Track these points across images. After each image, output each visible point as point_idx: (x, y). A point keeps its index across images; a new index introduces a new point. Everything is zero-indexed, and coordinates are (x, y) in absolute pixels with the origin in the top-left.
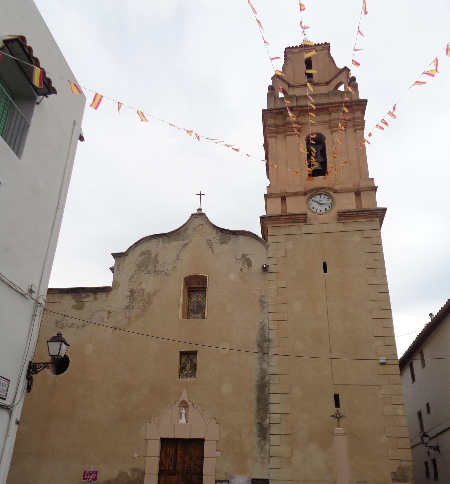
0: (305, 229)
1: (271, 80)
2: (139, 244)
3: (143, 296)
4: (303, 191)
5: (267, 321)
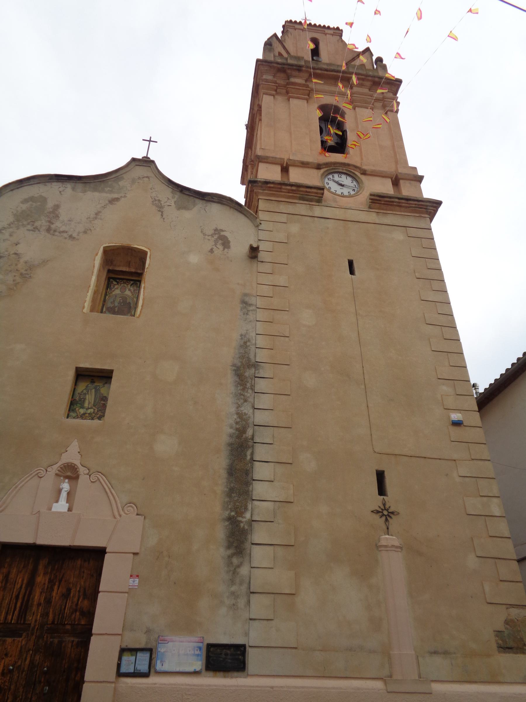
0: (318, 211)
3: (16, 265)
4: (316, 163)
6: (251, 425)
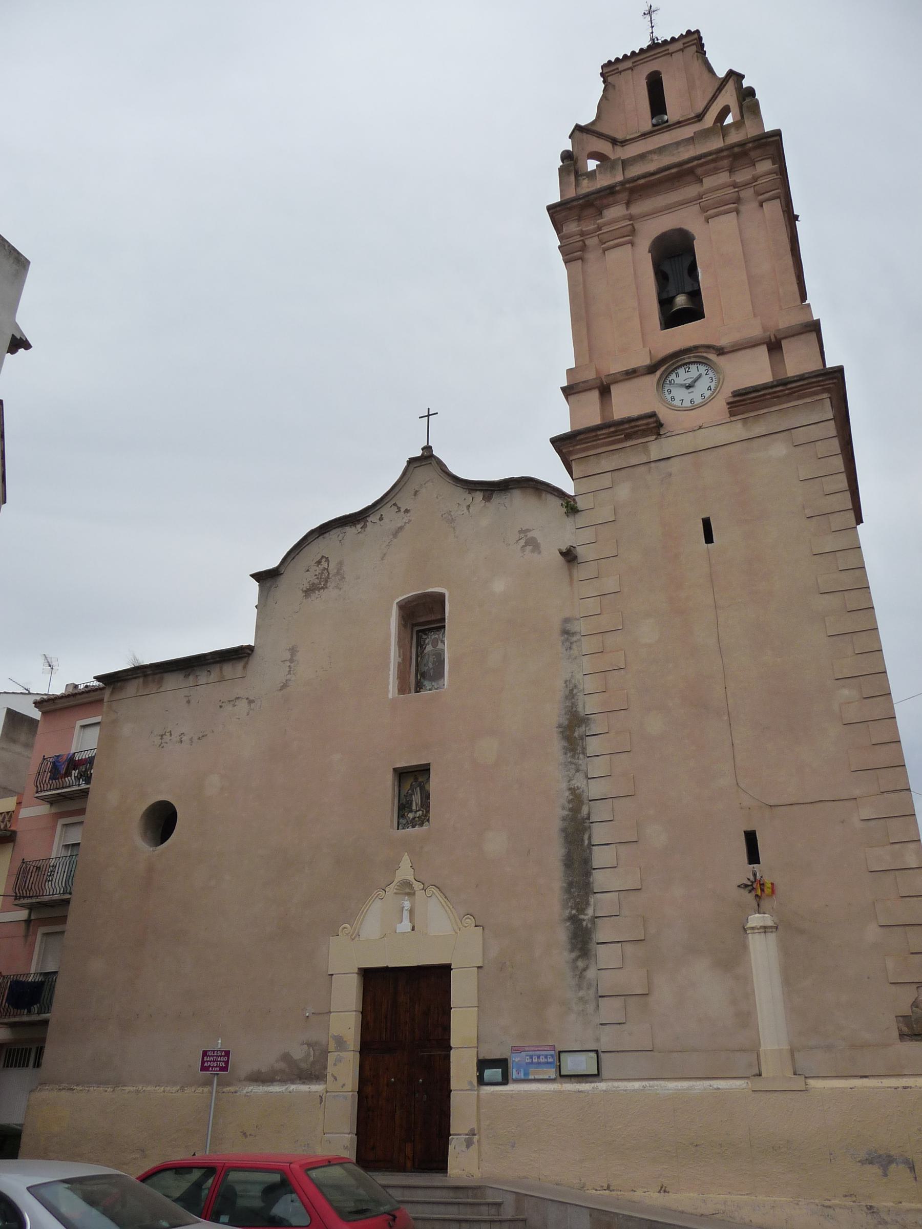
0: (657, 448)
1: (570, 140)
5: (579, 676)
6: (586, 801)
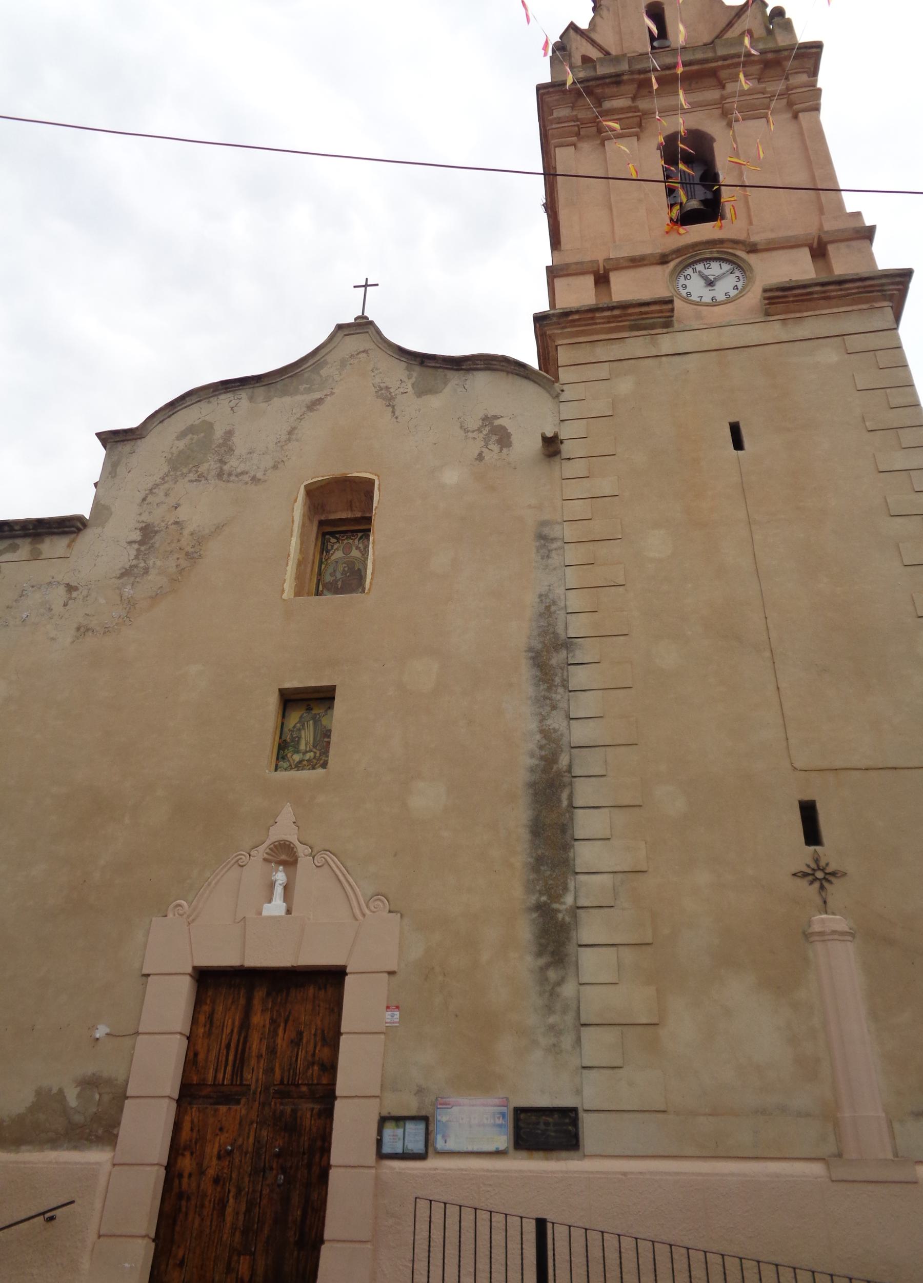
0: (666, 343)
2: (179, 408)
3: (179, 541)
5: (560, 591)
